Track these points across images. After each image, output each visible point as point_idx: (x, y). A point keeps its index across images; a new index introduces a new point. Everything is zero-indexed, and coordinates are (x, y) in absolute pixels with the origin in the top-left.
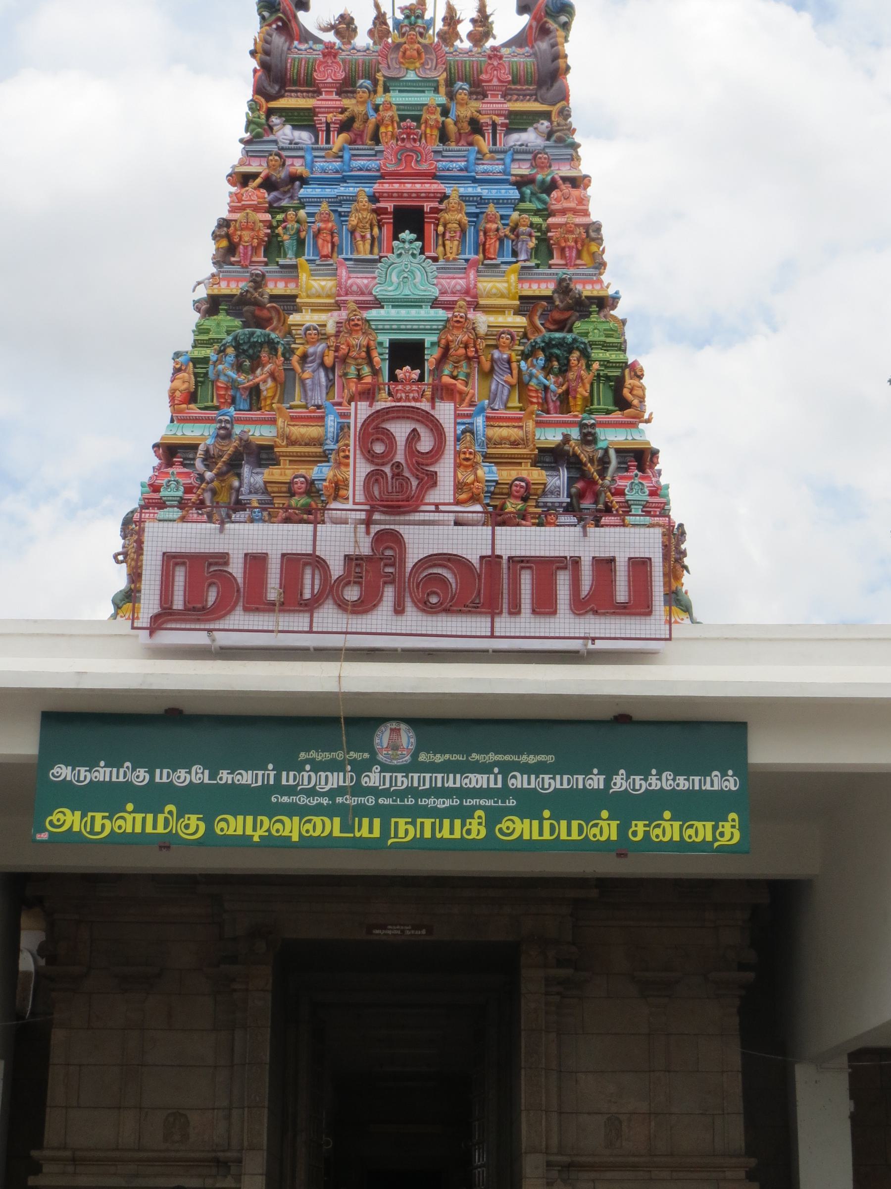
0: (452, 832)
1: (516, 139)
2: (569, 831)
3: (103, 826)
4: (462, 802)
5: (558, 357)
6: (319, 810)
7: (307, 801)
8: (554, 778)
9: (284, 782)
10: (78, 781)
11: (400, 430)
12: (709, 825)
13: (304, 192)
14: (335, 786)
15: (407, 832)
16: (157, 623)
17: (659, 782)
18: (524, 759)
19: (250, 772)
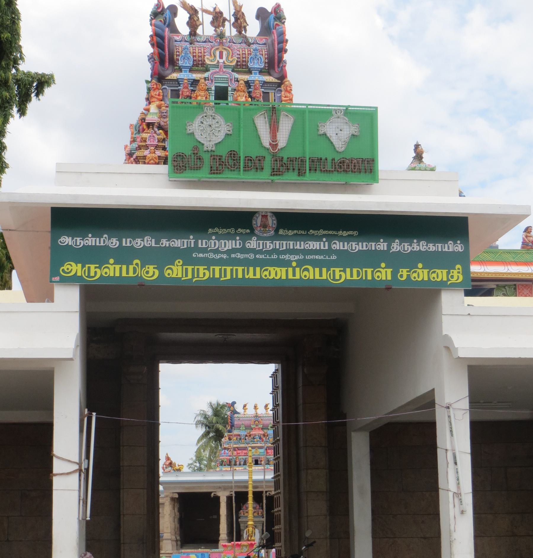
0: (255, 274)
3: (96, 273)
4: (305, 257)
6: (220, 262)
7: (214, 256)
8: (358, 244)
9: (200, 246)
10: (76, 245)
12: (445, 272)
14: (230, 248)
15: (204, 274)
17: (418, 247)
18: (340, 233)
19: (179, 240)
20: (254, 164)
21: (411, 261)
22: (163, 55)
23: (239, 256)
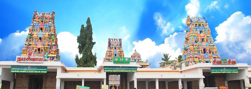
1: (50, 23)
2: (38, 72)
5: (50, 38)
11: (30, 51)
13: (35, 27)
16: (17, 61)
20: (120, 62)
21: (132, 70)
22: (110, 44)
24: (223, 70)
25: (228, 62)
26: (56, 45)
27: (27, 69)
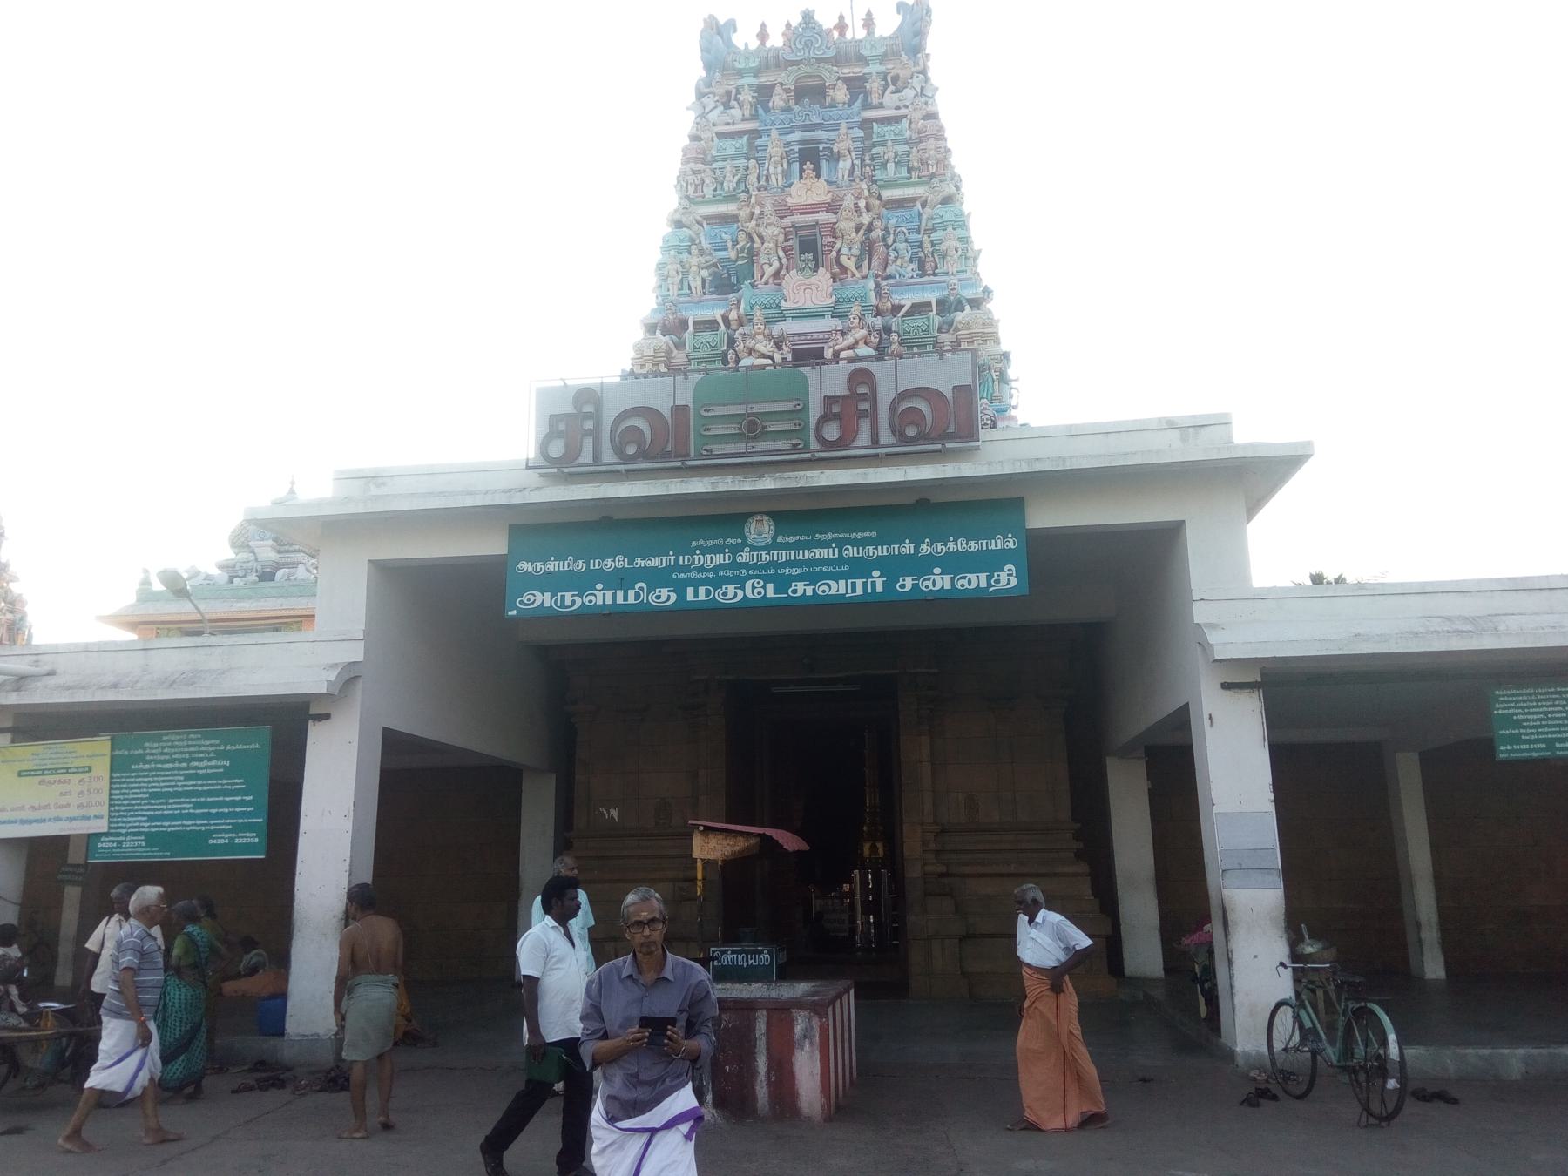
23: (729, 573)
24: (717, 560)
25: (814, 413)
26: (924, 72)
27: (736, 550)
